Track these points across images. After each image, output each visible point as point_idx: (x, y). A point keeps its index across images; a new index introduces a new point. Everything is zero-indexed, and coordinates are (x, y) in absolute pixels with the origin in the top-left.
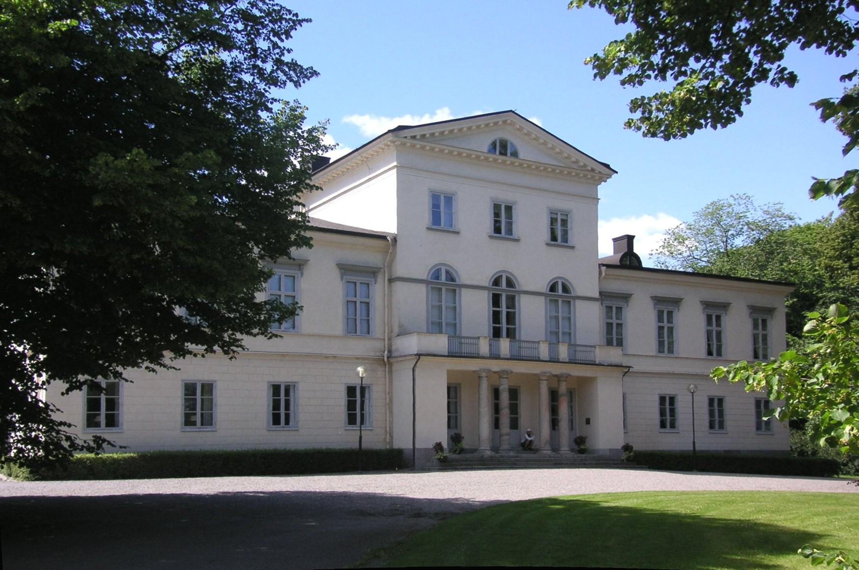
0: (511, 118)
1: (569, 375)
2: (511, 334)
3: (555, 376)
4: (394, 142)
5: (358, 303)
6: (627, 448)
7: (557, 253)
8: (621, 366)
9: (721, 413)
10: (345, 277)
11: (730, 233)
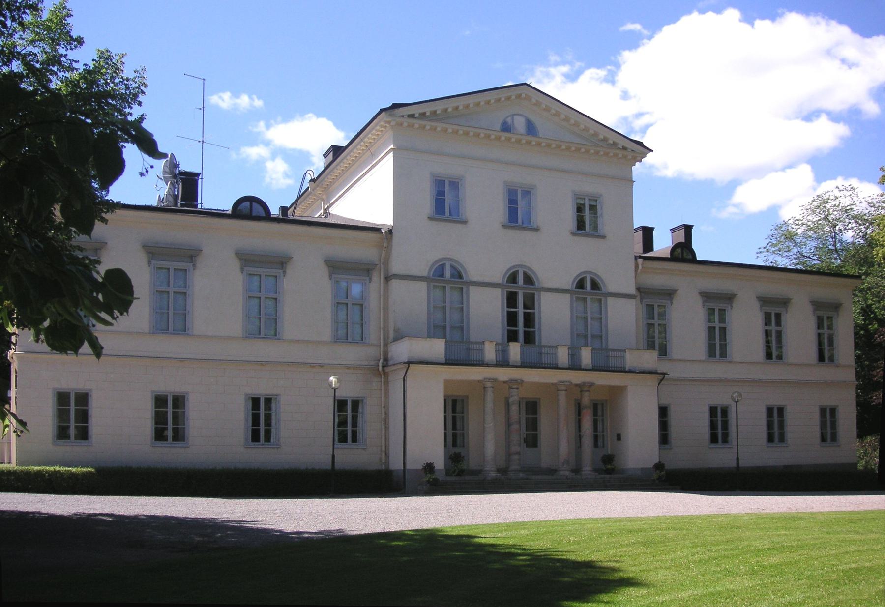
0: (524, 90)
1: (592, 385)
2: (529, 339)
3: (577, 385)
4: (389, 122)
5: (171, 295)
6: (659, 466)
7: (586, 244)
8: (656, 373)
9: (834, 425)
10: (246, 269)
11: (837, 228)
